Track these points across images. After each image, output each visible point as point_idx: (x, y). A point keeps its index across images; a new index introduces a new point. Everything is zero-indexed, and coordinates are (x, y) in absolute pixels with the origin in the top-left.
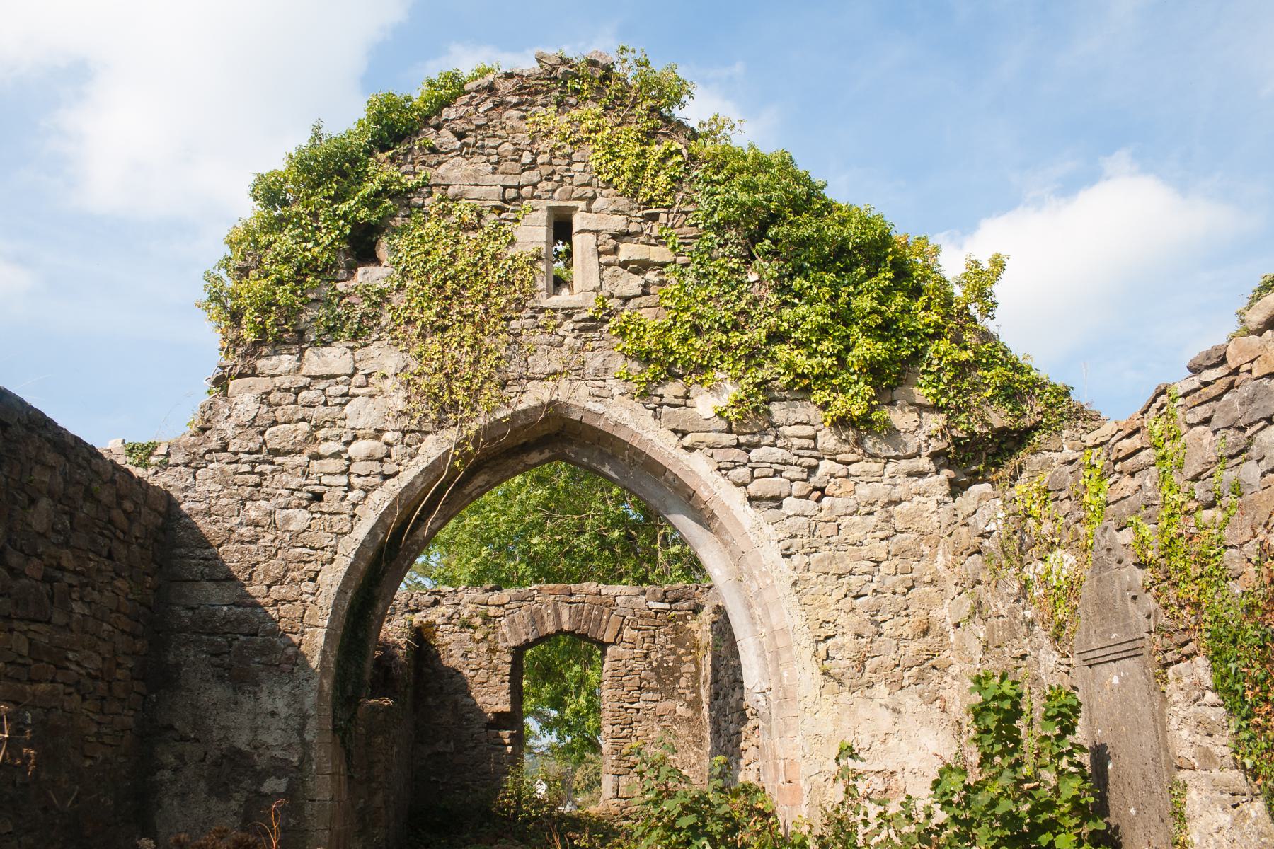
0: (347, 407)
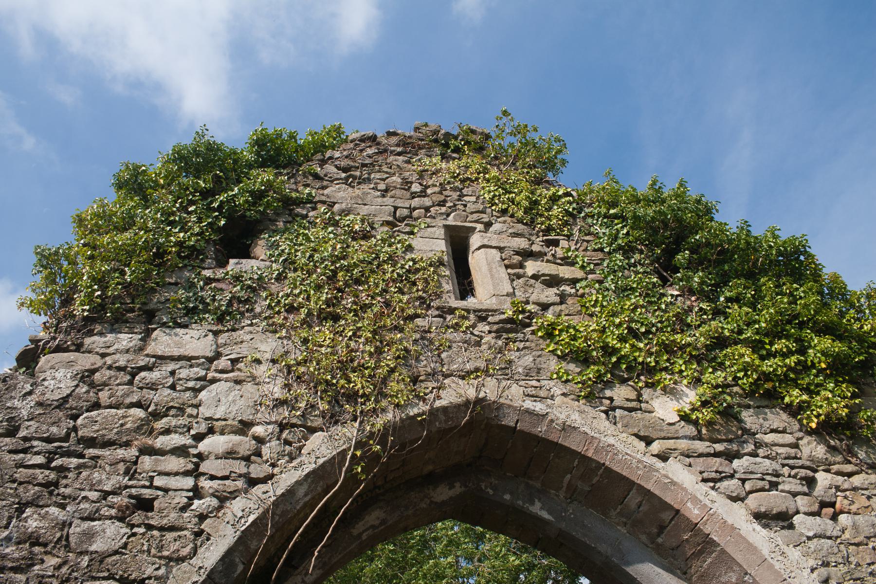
0: (203, 393)
